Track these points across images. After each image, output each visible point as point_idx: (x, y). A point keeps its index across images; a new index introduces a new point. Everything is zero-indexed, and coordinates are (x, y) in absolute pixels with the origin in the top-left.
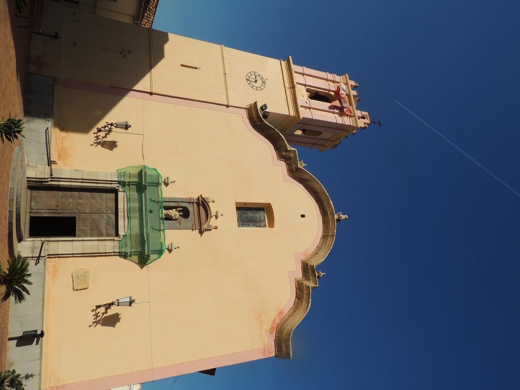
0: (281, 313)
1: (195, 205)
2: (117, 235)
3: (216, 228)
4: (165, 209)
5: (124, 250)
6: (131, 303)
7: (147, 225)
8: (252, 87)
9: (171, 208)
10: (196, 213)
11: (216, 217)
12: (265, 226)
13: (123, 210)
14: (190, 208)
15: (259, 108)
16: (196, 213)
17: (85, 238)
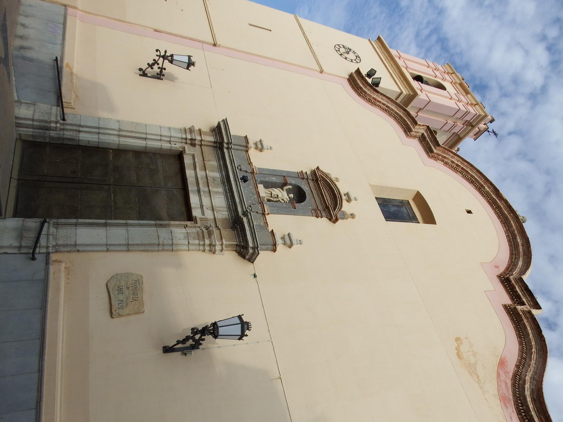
0: (502, 363)
2: (190, 217)
4: (267, 185)
5: (189, 137)
6: (190, 64)
8: (346, 58)
10: (319, 195)
13: (195, 188)
14: (305, 188)
16: (319, 195)
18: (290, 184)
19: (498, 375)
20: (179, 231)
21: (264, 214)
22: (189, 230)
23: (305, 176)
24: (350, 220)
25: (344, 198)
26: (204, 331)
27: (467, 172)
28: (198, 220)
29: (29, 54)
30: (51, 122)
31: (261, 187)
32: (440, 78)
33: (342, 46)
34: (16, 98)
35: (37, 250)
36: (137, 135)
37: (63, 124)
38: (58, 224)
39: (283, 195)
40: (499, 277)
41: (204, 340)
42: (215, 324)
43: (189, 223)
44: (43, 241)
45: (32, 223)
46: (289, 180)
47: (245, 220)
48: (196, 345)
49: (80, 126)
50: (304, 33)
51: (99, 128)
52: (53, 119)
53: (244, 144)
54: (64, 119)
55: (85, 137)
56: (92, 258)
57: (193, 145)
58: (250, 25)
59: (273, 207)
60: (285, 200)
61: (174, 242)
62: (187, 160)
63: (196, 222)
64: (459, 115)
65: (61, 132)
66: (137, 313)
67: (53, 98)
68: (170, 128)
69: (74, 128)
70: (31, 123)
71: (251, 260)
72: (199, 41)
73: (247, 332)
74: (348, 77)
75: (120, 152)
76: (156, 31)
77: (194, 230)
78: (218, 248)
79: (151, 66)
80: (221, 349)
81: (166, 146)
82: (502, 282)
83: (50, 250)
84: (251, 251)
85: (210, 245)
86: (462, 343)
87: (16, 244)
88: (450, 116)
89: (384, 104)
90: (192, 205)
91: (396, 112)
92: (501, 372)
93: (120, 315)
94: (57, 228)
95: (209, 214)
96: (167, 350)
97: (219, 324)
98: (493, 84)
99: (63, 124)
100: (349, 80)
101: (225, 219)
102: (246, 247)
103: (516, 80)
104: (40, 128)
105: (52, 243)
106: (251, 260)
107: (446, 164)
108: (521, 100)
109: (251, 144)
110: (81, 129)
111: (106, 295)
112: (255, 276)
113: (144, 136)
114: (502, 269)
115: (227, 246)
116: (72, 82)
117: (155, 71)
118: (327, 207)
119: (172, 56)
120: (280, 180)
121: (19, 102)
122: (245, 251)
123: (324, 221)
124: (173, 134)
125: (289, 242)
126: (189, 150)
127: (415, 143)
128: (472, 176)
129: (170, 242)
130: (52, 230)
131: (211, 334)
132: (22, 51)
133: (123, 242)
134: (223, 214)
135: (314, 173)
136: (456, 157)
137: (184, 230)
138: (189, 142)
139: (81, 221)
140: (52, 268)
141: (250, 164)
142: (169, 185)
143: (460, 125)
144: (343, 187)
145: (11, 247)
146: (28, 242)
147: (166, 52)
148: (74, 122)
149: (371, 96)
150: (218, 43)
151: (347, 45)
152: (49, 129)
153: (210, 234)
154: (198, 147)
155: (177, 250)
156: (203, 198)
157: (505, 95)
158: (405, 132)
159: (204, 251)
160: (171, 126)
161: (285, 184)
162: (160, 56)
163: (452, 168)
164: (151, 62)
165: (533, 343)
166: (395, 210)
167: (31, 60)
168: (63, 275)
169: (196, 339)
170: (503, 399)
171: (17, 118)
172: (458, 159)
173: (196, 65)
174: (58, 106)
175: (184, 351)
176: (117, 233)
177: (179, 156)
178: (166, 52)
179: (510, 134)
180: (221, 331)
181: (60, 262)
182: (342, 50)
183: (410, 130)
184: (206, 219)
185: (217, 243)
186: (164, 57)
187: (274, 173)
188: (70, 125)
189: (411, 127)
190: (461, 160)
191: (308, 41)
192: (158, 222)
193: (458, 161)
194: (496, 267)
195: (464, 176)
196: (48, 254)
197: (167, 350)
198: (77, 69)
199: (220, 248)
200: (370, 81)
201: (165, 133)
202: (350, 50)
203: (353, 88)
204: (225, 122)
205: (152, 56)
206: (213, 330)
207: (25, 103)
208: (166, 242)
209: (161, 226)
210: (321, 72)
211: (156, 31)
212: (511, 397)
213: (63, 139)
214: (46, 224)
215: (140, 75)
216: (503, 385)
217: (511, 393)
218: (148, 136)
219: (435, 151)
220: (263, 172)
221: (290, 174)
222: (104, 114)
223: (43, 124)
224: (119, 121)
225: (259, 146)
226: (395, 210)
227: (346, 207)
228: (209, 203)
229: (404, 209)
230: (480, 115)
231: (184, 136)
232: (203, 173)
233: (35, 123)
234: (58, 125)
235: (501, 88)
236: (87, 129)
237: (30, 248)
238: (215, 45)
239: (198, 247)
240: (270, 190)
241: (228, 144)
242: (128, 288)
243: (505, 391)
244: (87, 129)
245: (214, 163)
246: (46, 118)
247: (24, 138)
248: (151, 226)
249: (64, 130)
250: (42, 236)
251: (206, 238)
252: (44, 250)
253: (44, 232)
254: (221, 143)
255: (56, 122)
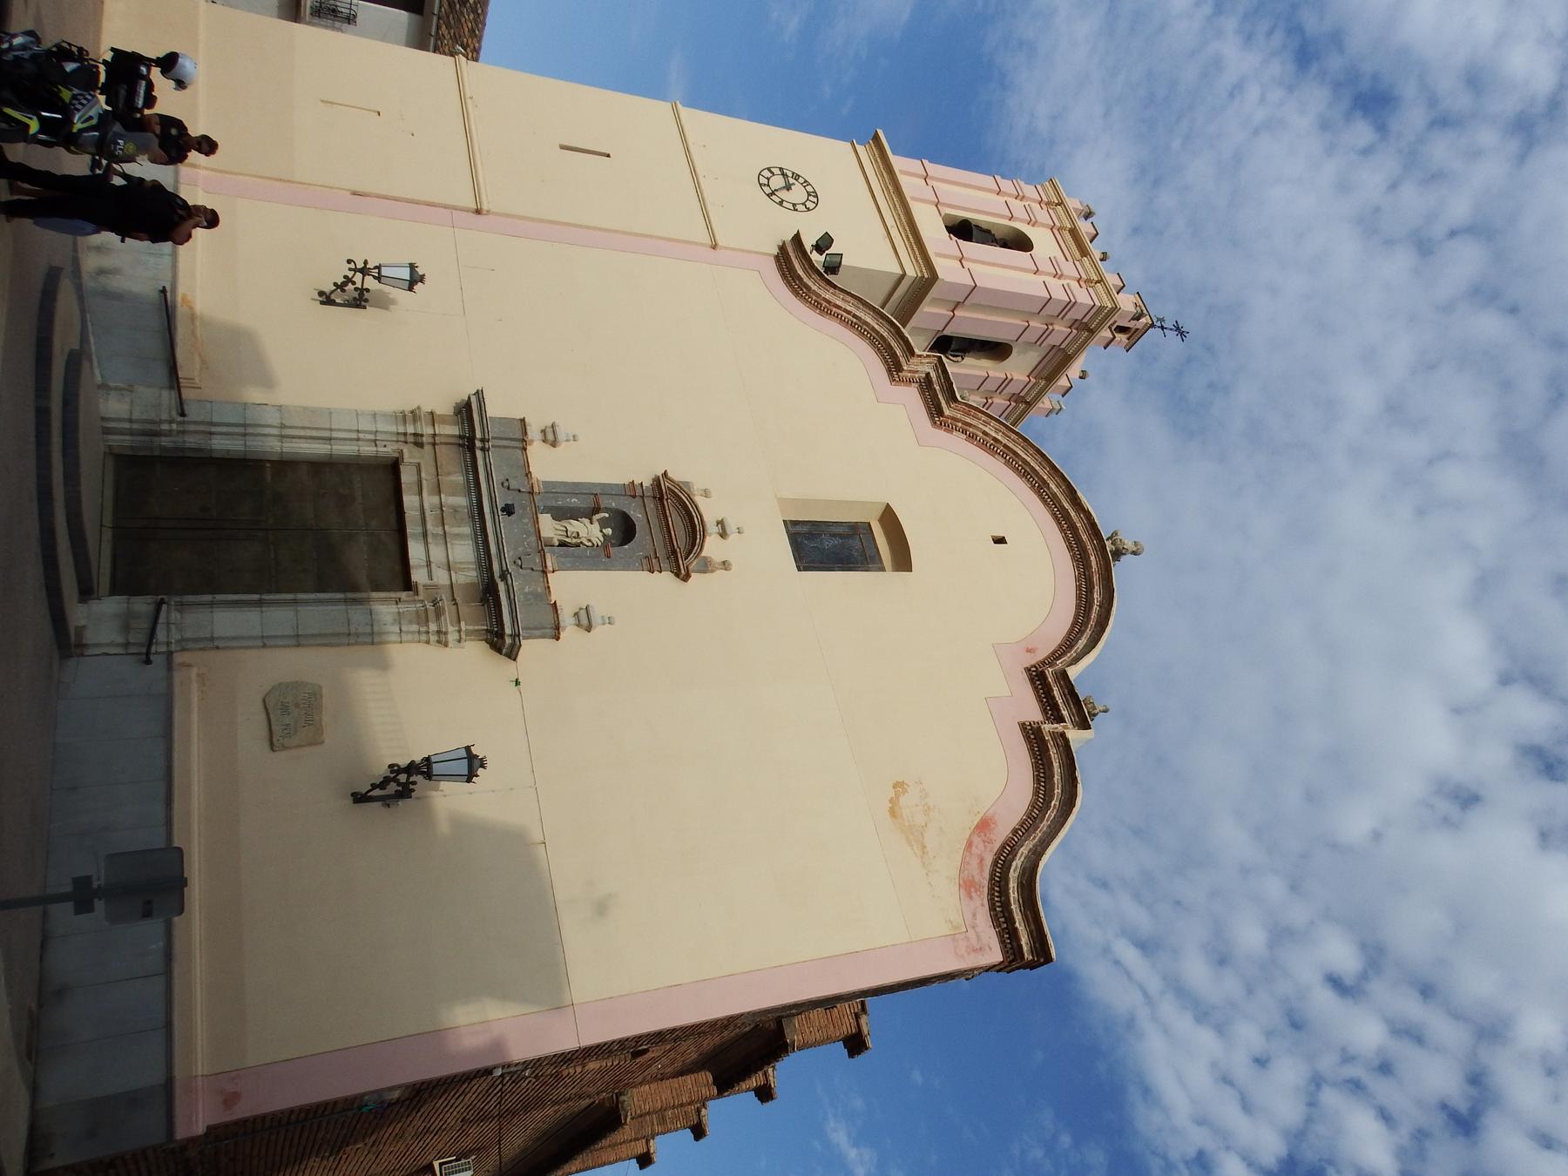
0: (984, 826)
1: (650, 504)
2: (408, 585)
3: (725, 565)
4: (560, 514)
5: (410, 430)
6: (415, 280)
7: (489, 476)
8: (781, 203)
9: (575, 514)
10: (658, 527)
11: (723, 535)
12: (883, 569)
13: (419, 530)
14: (637, 515)
15: (808, 248)
16: (658, 527)
17: (301, 596)
18: (607, 510)
19: (969, 845)
20: (386, 609)
21: (544, 572)
22: (402, 608)
23: (639, 492)
24: (720, 573)
25: (712, 528)
26: (412, 768)
27: (1015, 453)
28: (420, 588)
29: (116, 283)
30: (161, 422)
31: (546, 521)
32: (1022, 221)
33: (776, 171)
34: (99, 379)
35: (153, 649)
36: (314, 433)
37: (183, 423)
38: (182, 604)
39: (590, 531)
40: (1028, 670)
41: (414, 783)
42: (428, 759)
43: (403, 595)
44: (161, 635)
45: (142, 605)
46: (605, 502)
47: (501, 586)
48: (405, 792)
49: (212, 424)
50: (687, 150)
51: (244, 425)
52: (165, 416)
53: (519, 435)
54: (183, 414)
55: (221, 445)
56: (238, 658)
57: (420, 445)
58: (563, 147)
59: (566, 556)
60: (595, 540)
61: (376, 629)
62: (407, 476)
63: (417, 593)
64: (1052, 310)
65: (179, 439)
66: (310, 744)
67: (161, 373)
68: (375, 415)
69: (202, 428)
70: (127, 425)
71: (512, 655)
72: (445, 207)
73: (480, 771)
74: (775, 251)
75: (286, 465)
76: (355, 193)
77: (412, 608)
78: (453, 637)
79: (340, 287)
80: (448, 798)
81: (367, 450)
82: (1032, 680)
83: (173, 647)
84: (508, 641)
85: (439, 632)
86: (905, 791)
87: (120, 640)
88: (1032, 314)
89: (849, 312)
90: (412, 562)
91: (873, 329)
92: (977, 840)
93: (285, 748)
94: (181, 612)
95: (441, 577)
96: (360, 798)
97: (433, 759)
98: (1409, 90)
99: (183, 423)
100: (777, 258)
101: (472, 584)
102: (500, 634)
103: (1476, 79)
104: (144, 433)
105: (175, 636)
106: (512, 655)
107: (972, 437)
108: (1487, 137)
109: (534, 433)
110: (213, 429)
111: (263, 716)
112: (517, 683)
113: (327, 434)
114: (1041, 655)
115: (468, 633)
116: (193, 333)
117: (352, 293)
118: (674, 552)
119: (378, 267)
120: (588, 503)
121: (104, 386)
122: (501, 642)
123: (667, 577)
124: (381, 427)
125: (585, 621)
126: (410, 455)
127: (911, 395)
128: (1024, 461)
129: (368, 630)
130: (175, 616)
131: (422, 773)
132: (102, 279)
133: (289, 632)
134: (468, 575)
135: (657, 482)
136: (993, 423)
137: (393, 609)
138: (410, 439)
139: (219, 597)
140: (178, 677)
141: (528, 474)
142: (374, 523)
143: (1061, 329)
144: (710, 511)
145: (112, 644)
146: (138, 637)
147: (366, 262)
148: (201, 418)
149: (819, 296)
150: (485, 207)
151: (791, 166)
152: (158, 434)
153: (439, 614)
154: (428, 448)
155: (381, 643)
156: (431, 547)
157: (1443, 122)
158: (889, 371)
159: (428, 642)
160: (376, 409)
161: (597, 510)
162: (355, 270)
163: (983, 445)
164: (340, 280)
165: (1057, 791)
166: (827, 545)
167: (119, 296)
168: (195, 686)
169: (404, 783)
170: (968, 886)
171: (103, 419)
172: (998, 426)
173: (427, 279)
174: (171, 388)
175: (386, 801)
176: (279, 617)
177: (394, 466)
178: (366, 262)
179: (1453, 234)
180: (436, 769)
181: (189, 666)
182: (777, 182)
183: (899, 368)
184: (436, 587)
185: (451, 629)
186: (364, 271)
187: (575, 489)
188: (195, 423)
189: (902, 360)
190: (1003, 429)
191: (693, 172)
192: (350, 595)
193: (997, 431)
194: (1029, 651)
195: (1008, 463)
196: (170, 654)
197: (360, 798)
198: (199, 308)
199: (456, 636)
200: (817, 259)
201: (366, 425)
202: (797, 177)
203: (784, 276)
204: (479, 394)
205: (340, 272)
206: (424, 769)
207: (117, 389)
208: (361, 630)
209: (354, 601)
210: (714, 247)
211: (355, 193)
212: (986, 883)
213: (183, 449)
214: (164, 607)
215: (322, 303)
216: (975, 863)
217: (987, 875)
218: (335, 435)
219: (947, 412)
220: (552, 488)
221: (607, 490)
222: (254, 395)
223: (149, 427)
224: (280, 408)
225: (550, 437)
226: (827, 545)
227: (712, 547)
228: (442, 557)
229: (856, 543)
230: (1102, 308)
231: (401, 430)
232: (435, 499)
233: (135, 426)
234: (174, 426)
235: (1433, 101)
236: (224, 429)
237: (140, 645)
238: (478, 212)
239: (416, 637)
240: (564, 523)
241: (483, 440)
242: (297, 705)
243: (975, 872)
244: (224, 429)
245: (459, 478)
246: (152, 415)
247: (116, 451)
248: (338, 601)
249: (183, 432)
250: (159, 627)
251: (431, 620)
252: (163, 649)
253: (162, 619)
254: (472, 439)
255: (171, 422)
